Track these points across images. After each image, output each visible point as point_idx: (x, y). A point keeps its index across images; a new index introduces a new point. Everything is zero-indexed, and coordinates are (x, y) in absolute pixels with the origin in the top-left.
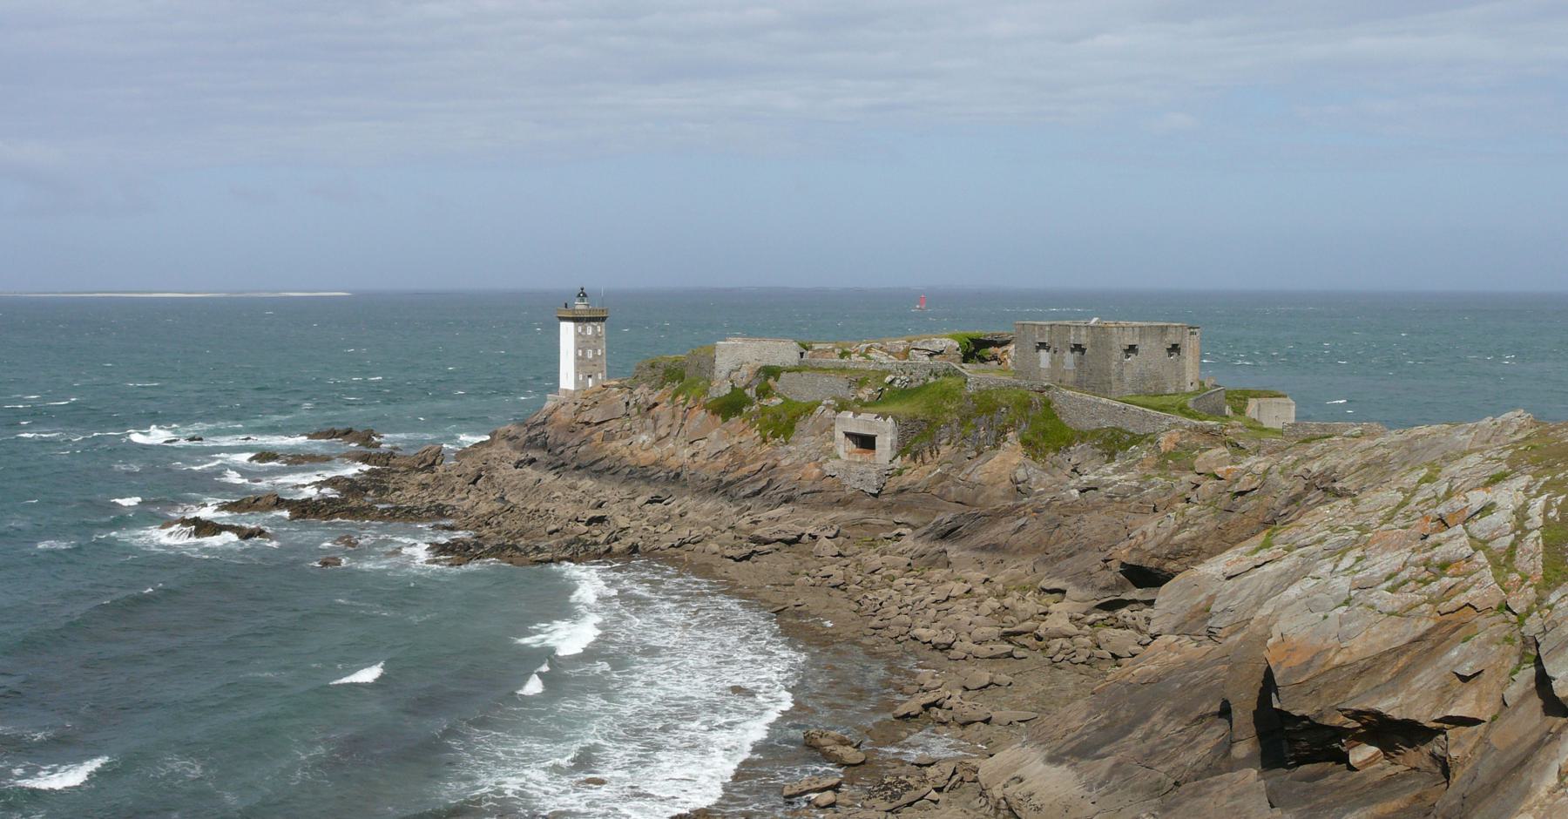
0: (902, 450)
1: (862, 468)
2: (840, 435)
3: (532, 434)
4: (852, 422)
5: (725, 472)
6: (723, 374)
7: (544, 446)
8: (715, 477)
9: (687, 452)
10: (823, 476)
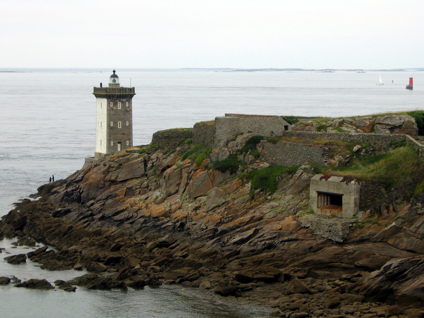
0: (362, 205)
1: (331, 221)
2: (313, 194)
3: (69, 189)
4: (319, 185)
5: (219, 224)
6: (222, 144)
7: (79, 200)
8: (211, 227)
9: (191, 205)
10: (299, 227)
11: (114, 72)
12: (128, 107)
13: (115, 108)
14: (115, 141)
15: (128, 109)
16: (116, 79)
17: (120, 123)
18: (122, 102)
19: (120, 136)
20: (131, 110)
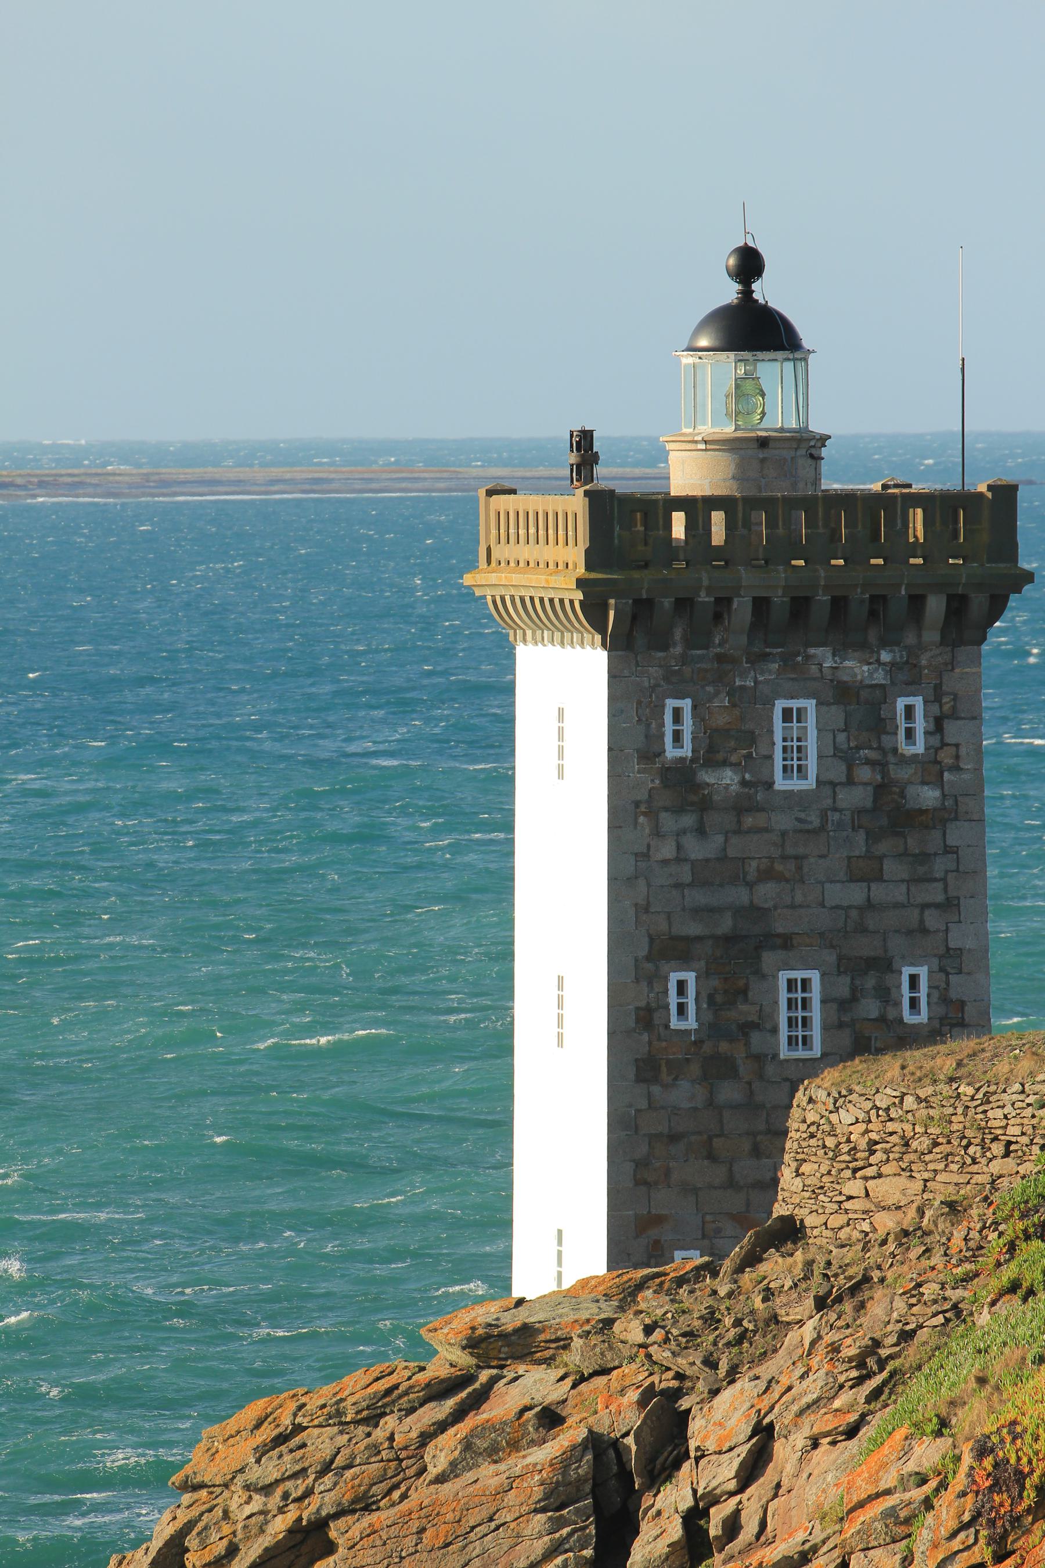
12: (931, 768)
15: (928, 796)
16: (772, 371)
18: (841, 693)
20: (961, 809)
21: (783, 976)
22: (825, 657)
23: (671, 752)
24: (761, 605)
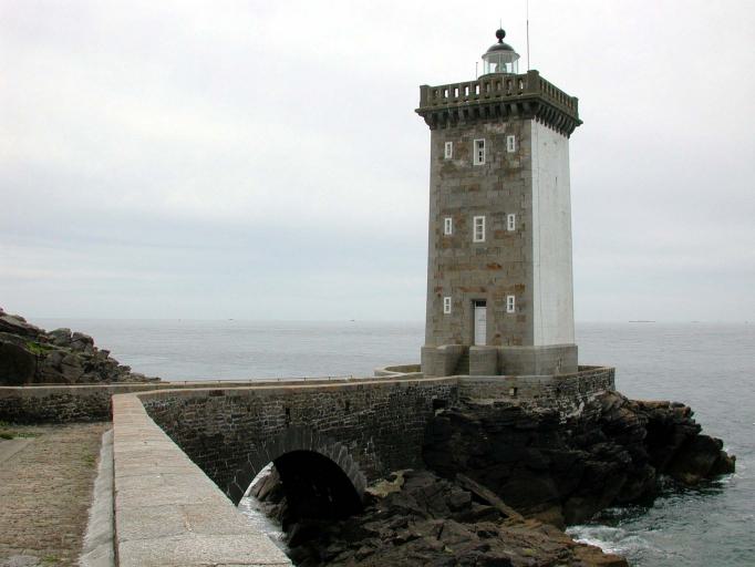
11: (501, 34)
12: (517, 156)
13: (461, 163)
14: (459, 295)
15: (515, 164)
17: (480, 221)
19: (483, 276)
20: (525, 167)
21: (475, 218)
22: (489, 127)
23: (446, 156)
24: (466, 112)
